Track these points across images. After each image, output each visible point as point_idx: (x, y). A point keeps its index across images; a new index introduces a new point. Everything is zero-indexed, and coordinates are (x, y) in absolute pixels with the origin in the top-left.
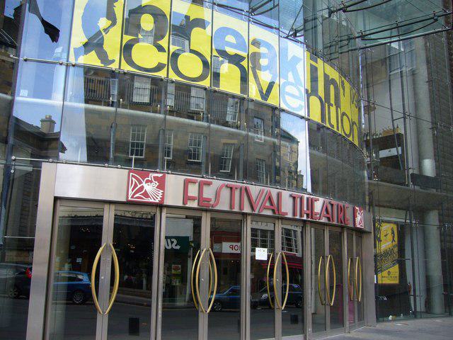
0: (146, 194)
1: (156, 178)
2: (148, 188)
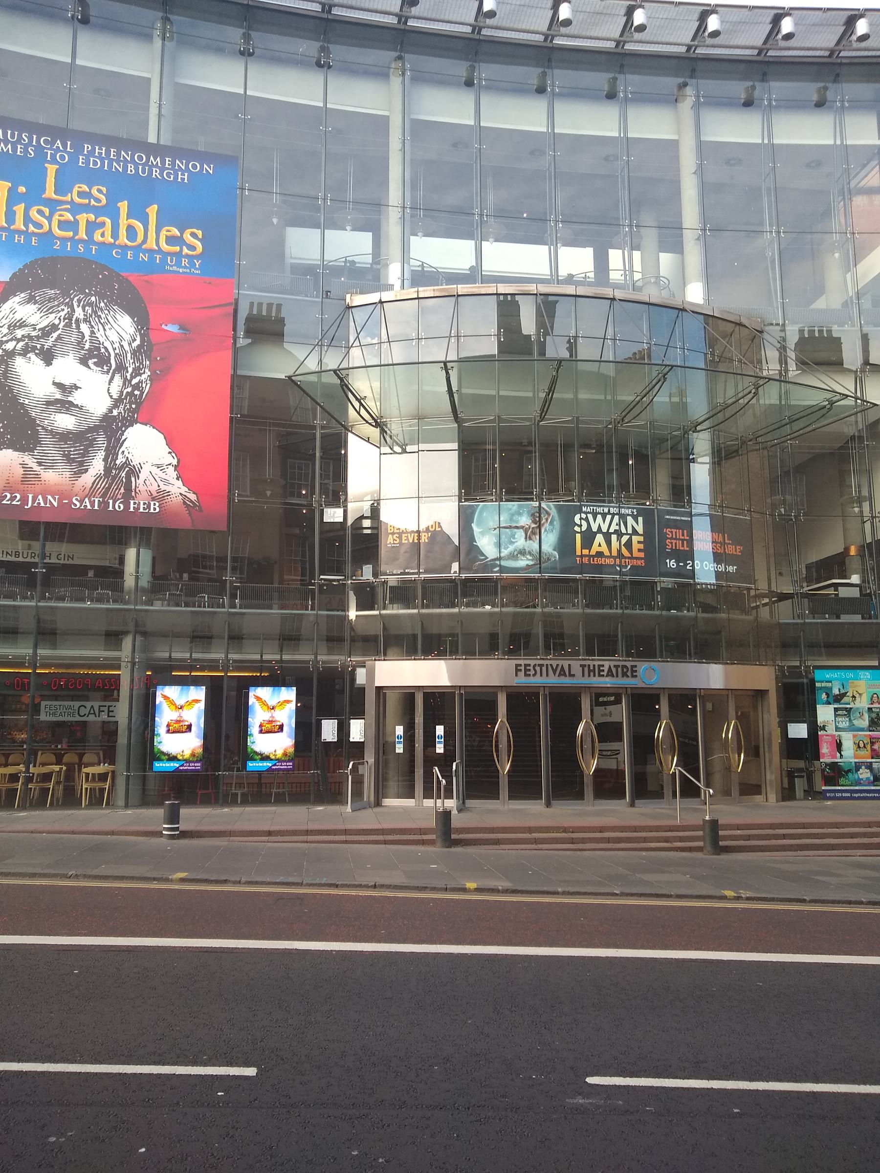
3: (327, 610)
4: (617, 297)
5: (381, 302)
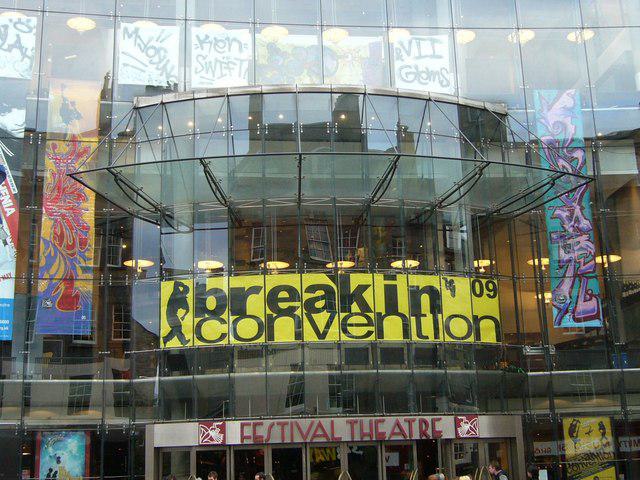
0: (211, 439)
1: (218, 426)
2: (213, 434)
3: (71, 378)
4: (368, 92)
5: (163, 103)
